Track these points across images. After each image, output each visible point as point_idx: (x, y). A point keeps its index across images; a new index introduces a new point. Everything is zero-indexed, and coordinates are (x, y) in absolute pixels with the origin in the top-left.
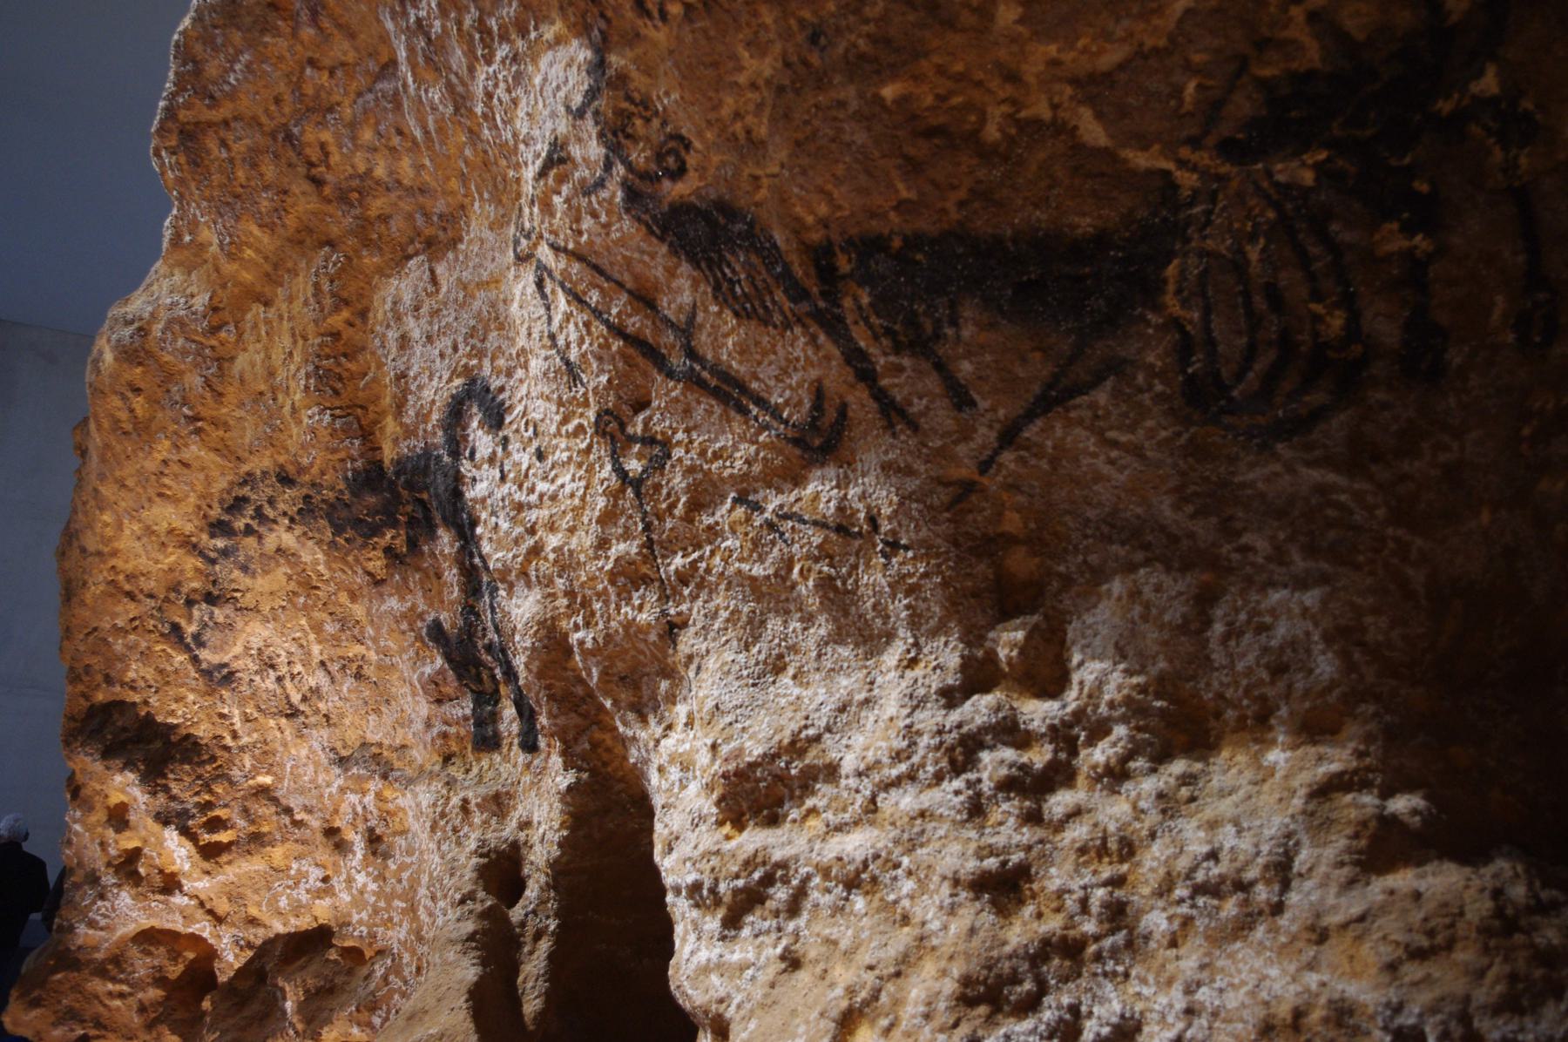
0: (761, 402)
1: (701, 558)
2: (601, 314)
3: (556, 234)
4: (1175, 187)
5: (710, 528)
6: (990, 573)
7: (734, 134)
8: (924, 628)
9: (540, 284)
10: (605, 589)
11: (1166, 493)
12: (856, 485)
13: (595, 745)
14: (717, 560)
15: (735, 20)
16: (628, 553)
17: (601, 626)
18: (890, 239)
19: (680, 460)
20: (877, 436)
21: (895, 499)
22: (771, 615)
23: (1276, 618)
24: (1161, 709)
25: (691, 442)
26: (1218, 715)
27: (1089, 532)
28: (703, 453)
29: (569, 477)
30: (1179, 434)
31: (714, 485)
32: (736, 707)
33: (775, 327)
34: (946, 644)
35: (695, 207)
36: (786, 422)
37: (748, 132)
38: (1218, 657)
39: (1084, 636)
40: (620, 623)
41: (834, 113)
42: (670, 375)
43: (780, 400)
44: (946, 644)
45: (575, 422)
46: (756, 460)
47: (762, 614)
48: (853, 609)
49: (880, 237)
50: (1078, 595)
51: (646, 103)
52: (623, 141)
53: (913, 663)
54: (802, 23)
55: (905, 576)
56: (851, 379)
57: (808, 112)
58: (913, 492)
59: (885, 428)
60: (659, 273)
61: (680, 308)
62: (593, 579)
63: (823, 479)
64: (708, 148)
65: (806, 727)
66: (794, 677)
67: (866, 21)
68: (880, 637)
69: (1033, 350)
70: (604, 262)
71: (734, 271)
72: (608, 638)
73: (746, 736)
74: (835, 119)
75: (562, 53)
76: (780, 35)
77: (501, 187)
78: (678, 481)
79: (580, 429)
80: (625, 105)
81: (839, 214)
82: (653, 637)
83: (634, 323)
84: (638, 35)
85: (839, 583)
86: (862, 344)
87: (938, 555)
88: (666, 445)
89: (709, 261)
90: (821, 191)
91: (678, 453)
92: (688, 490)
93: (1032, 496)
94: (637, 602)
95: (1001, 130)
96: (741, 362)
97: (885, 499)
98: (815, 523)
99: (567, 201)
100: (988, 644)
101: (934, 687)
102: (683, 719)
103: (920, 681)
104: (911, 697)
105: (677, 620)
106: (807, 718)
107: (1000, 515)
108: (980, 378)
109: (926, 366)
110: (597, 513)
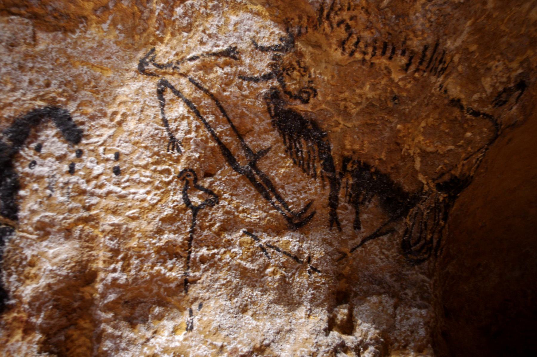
0: (279, 197)
1: (218, 253)
4: (422, 188)
5: (229, 241)
11: (389, 272)
12: (307, 243)
13: (68, 337)
14: (228, 256)
16: (175, 240)
17: (133, 272)
19: (224, 206)
20: (323, 228)
22: (245, 286)
23: (411, 316)
24: (382, 342)
25: (232, 200)
26: (392, 344)
28: (237, 208)
30: (397, 256)
31: (236, 223)
32: (230, 327)
33: (308, 175)
34: (322, 311)
37: (346, 107)
38: (398, 326)
42: (236, 169)
43: (290, 201)
44: (322, 311)
47: (242, 285)
48: (289, 291)
49: (370, 165)
51: (306, 69)
52: (285, 75)
54: (392, 92)
55: (315, 282)
57: (378, 117)
58: (329, 252)
63: (292, 237)
65: (265, 339)
66: (252, 316)
70: (228, 110)
71: (301, 146)
72: (135, 280)
73: (236, 342)
74: (386, 125)
78: (219, 215)
79: (167, 172)
80: (294, 63)
81: (361, 152)
82: (173, 285)
83: (226, 139)
85: (287, 279)
87: (329, 277)
88: (218, 198)
89: (291, 138)
91: (222, 203)
94: (170, 266)
96: (281, 180)
97: (318, 252)
98: (285, 253)
100: (334, 312)
109: (354, 211)
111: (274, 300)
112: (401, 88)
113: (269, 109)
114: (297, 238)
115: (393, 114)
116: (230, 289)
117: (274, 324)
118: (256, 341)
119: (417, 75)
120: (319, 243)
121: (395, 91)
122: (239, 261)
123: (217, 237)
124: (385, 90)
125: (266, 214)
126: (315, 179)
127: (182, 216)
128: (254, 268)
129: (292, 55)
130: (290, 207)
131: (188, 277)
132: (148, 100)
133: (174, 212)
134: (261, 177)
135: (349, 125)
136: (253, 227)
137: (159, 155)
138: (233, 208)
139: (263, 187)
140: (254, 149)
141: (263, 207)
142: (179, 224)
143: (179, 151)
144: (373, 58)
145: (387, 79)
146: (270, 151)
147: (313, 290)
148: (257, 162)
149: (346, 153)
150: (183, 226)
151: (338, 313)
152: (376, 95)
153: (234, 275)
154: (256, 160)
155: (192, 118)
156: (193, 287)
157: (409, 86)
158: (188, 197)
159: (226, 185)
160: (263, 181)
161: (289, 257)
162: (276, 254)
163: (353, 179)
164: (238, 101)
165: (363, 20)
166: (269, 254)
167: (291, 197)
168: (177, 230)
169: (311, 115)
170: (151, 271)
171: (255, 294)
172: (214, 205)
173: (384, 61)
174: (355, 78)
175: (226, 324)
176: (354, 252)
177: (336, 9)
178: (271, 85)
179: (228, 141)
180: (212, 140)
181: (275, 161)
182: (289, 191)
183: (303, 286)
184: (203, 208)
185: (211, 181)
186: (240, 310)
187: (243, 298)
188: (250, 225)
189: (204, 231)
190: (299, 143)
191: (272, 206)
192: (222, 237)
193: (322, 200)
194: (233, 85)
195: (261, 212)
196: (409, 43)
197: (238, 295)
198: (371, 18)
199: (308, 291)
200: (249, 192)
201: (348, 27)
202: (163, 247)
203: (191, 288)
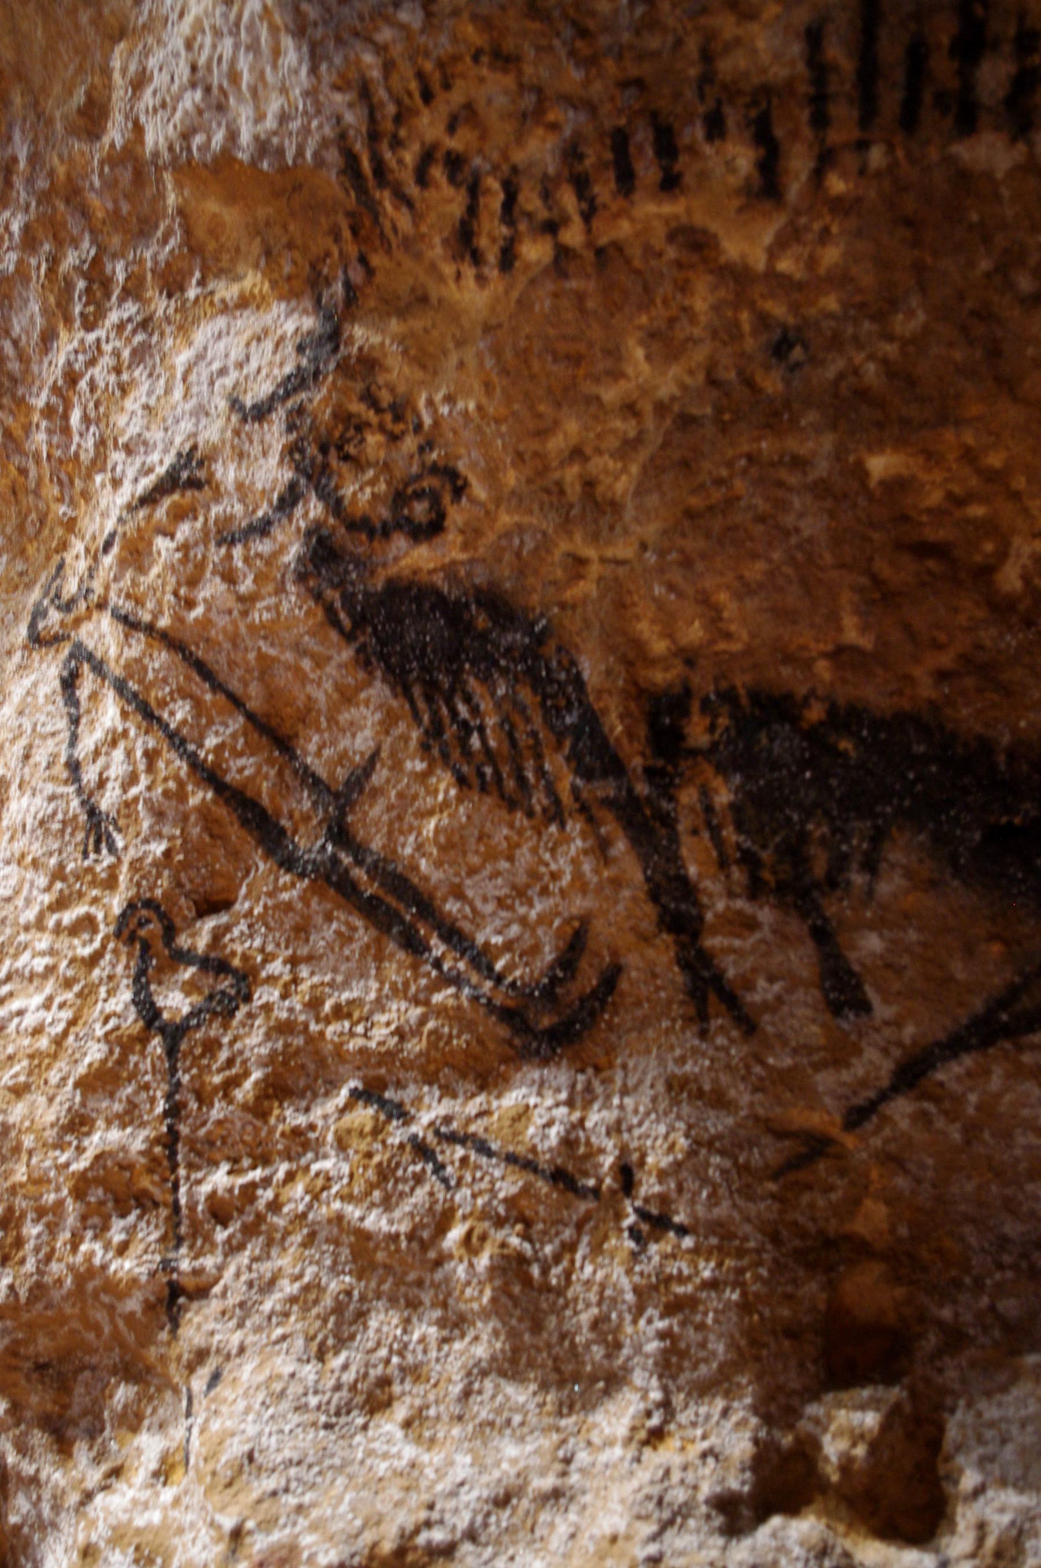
0: (453, 935)
1: (266, 1182)
2: (183, 742)
3: (139, 602)
5: (297, 1132)
6: (822, 1299)
7: (559, 484)
8: (682, 1379)
9: (69, 683)
10: (60, 1203)
12: (607, 1105)
14: (298, 1189)
15: (647, 289)
16: (124, 1149)
17: (30, 1266)
18: (806, 702)
19: (267, 1008)
20: (668, 1032)
21: (683, 1142)
22: (380, 1304)
25: (296, 981)
27: (1007, 1259)
28: (314, 1004)
29: (38, 999)
31: (322, 1062)
32: (289, 1463)
33: (530, 814)
34: (725, 1413)
35: (437, 593)
36: (499, 979)
37: (589, 484)
39: (980, 1440)
40: (71, 1268)
41: (783, 474)
42: (288, 863)
43: (497, 940)
44: (725, 1413)
45: (80, 910)
46: (416, 1032)
47: (363, 1298)
48: (552, 1322)
49: (789, 696)
50: (973, 1364)
51: (400, 410)
52: (334, 463)
53: (656, 1437)
54: (763, 320)
55: (668, 1280)
56: (647, 926)
57: (730, 464)
58: (719, 1137)
59: (688, 1020)
60: (321, 695)
61: (343, 757)
62: (39, 1181)
63: (541, 1087)
64: (498, 501)
65: (428, 1524)
66: (407, 1424)
67: (890, 338)
68: (593, 1379)
69: (992, 938)
70: (218, 661)
71: (475, 711)
73: (302, 1522)
74: (780, 484)
75: (248, 322)
76: (715, 334)
77: (30, 530)
79: (87, 923)
80: (357, 407)
81: (722, 646)
82: (133, 1305)
84: (424, 299)
85: (535, 1271)
86: (692, 870)
87: (740, 1253)
89: (431, 690)
90: (705, 600)
92: (271, 1059)
93: (918, 1181)
95: (1026, 578)
96: (438, 864)
98: (511, 1159)
99: (185, 548)
100: (804, 1426)
101: (706, 1490)
102: (150, 1460)
103: (676, 1476)
104: (660, 1502)
105: (189, 1283)
106: (431, 1507)
107: (856, 1202)
108: (888, 966)
109: (796, 926)
110: (81, 1069)
111: (493, 1358)
112: (800, 286)
113: (330, 610)
114: (558, 1090)
115: (794, 421)
116: (318, 1316)
117: (489, 1461)
118: (383, 1527)
119: (837, 184)
120: (654, 1100)
121: (778, 309)
122: (337, 1205)
123: (258, 1123)
124: (730, 333)
125: (419, 1011)
126: (562, 825)
127: (136, 1065)
128: (393, 1229)
129: (334, 382)
130: (499, 965)
131: (175, 1276)
132: (43, 718)
133: (111, 1052)
134: (373, 871)
135: (624, 550)
136: (383, 1071)
137: (64, 879)
138: (298, 1007)
139: (388, 907)
140: (332, 774)
141: (406, 984)
142: (129, 1090)
143: (112, 848)
144: (596, 223)
145: (709, 278)
146: (378, 766)
147: (662, 1317)
148: (350, 819)
149: (659, 677)
150: (144, 1095)
151: (825, 1430)
152: (691, 372)
153: (328, 1262)
154: (343, 814)
155: (132, 733)
156: (197, 1313)
157: (831, 255)
158: (149, 995)
159: (268, 927)
160: (382, 885)
161: (531, 1177)
162: (477, 1167)
163: (726, 781)
164: (234, 623)
165: (501, 101)
166: (449, 1169)
167: (498, 923)
168: (127, 1112)
169: (469, 574)
170: (71, 1260)
171: (416, 1336)
172: (237, 1008)
173: (651, 208)
174: (563, 347)
175: (278, 1450)
176: (869, 1126)
177: (388, 125)
178: (302, 524)
179: (247, 773)
180: (197, 785)
181: (400, 795)
182: (485, 899)
183: (614, 1300)
184: (198, 1026)
185: (214, 928)
186: (360, 1399)
187: (374, 1350)
188: (367, 1065)
189: (211, 1105)
190: (468, 699)
191: (434, 973)
192: (272, 1121)
193: (620, 907)
194: (208, 575)
195: (403, 1005)
196: (726, 66)
197: (352, 1337)
198: (528, 70)
199: (642, 1322)
200: (350, 939)
201: (455, 163)
202: (90, 1174)
203: (188, 1315)
